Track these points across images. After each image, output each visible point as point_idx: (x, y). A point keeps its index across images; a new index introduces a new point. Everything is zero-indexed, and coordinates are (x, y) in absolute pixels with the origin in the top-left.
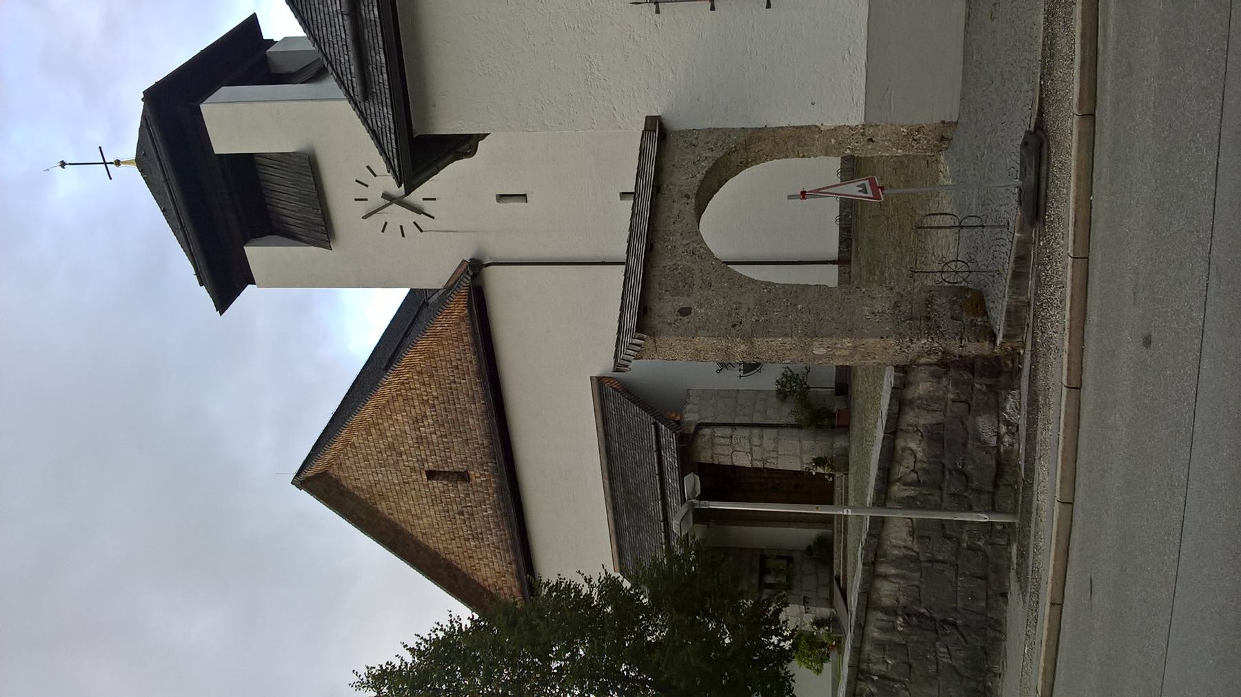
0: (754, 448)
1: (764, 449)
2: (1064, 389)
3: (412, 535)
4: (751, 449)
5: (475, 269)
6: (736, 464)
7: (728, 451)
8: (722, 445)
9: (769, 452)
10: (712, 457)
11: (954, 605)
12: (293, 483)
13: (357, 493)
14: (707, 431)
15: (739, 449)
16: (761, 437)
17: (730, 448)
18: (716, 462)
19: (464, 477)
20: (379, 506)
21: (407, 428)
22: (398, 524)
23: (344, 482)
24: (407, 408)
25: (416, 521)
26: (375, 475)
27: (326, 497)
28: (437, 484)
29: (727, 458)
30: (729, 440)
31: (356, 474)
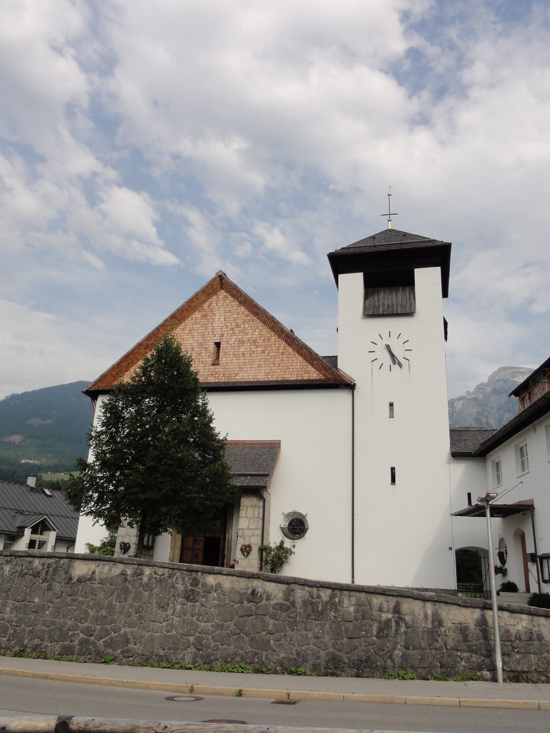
0: (252, 531)
1: (251, 537)
2: (458, 700)
3: (176, 328)
4: (251, 529)
5: (350, 386)
6: (240, 519)
7: (250, 514)
8: (254, 512)
9: (249, 539)
10: (244, 506)
11: (411, 648)
12: (409, 313)
13: (208, 303)
14: (261, 504)
15: (250, 522)
16: (258, 536)
17: (251, 517)
18: (241, 508)
19: (216, 362)
20: (197, 313)
21: (249, 336)
22: (184, 321)
23: (215, 297)
24: (262, 338)
25: (186, 332)
26: (219, 314)
27: (210, 286)
28: (212, 347)
29: (244, 514)
30: (257, 516)
31: (220, 304)
